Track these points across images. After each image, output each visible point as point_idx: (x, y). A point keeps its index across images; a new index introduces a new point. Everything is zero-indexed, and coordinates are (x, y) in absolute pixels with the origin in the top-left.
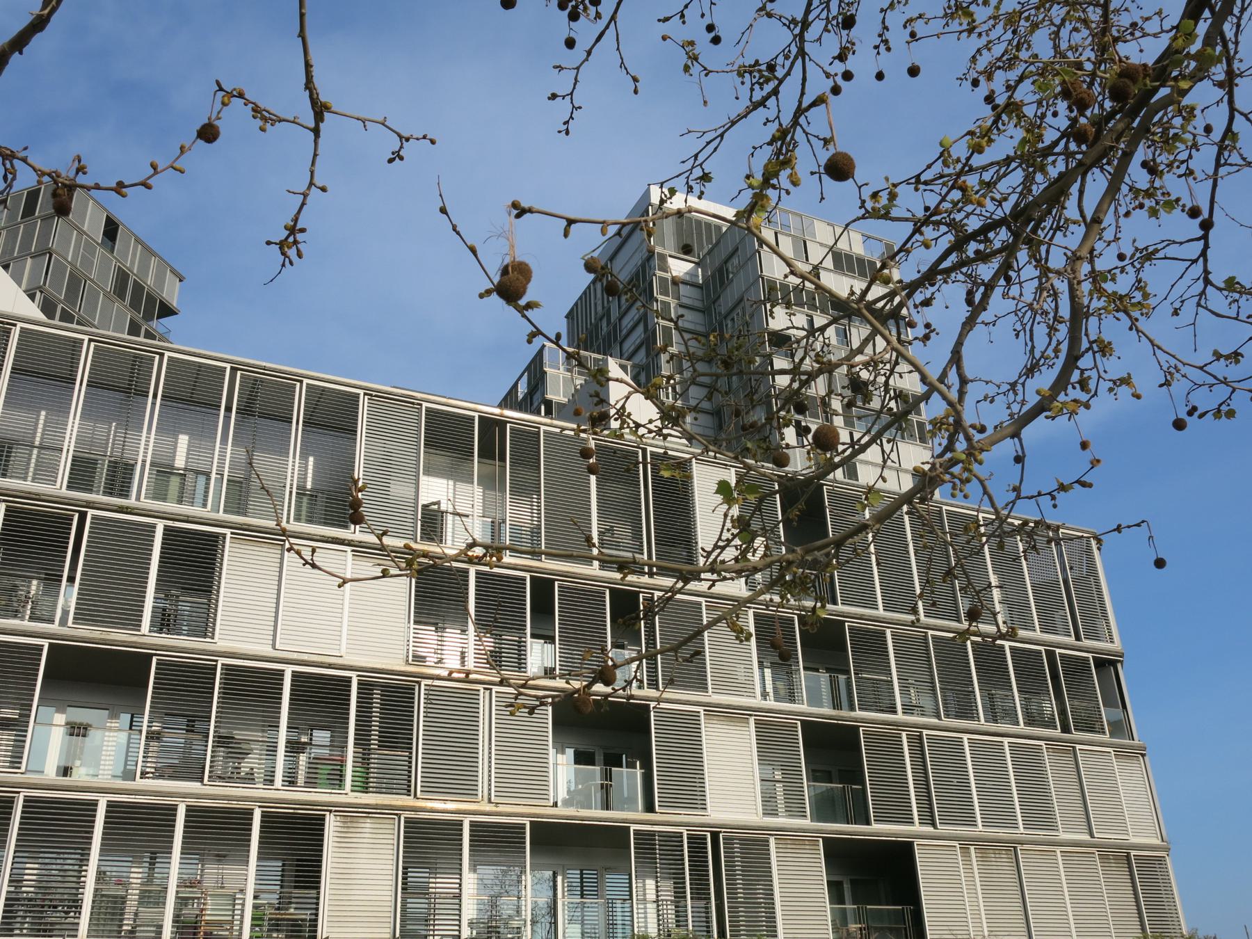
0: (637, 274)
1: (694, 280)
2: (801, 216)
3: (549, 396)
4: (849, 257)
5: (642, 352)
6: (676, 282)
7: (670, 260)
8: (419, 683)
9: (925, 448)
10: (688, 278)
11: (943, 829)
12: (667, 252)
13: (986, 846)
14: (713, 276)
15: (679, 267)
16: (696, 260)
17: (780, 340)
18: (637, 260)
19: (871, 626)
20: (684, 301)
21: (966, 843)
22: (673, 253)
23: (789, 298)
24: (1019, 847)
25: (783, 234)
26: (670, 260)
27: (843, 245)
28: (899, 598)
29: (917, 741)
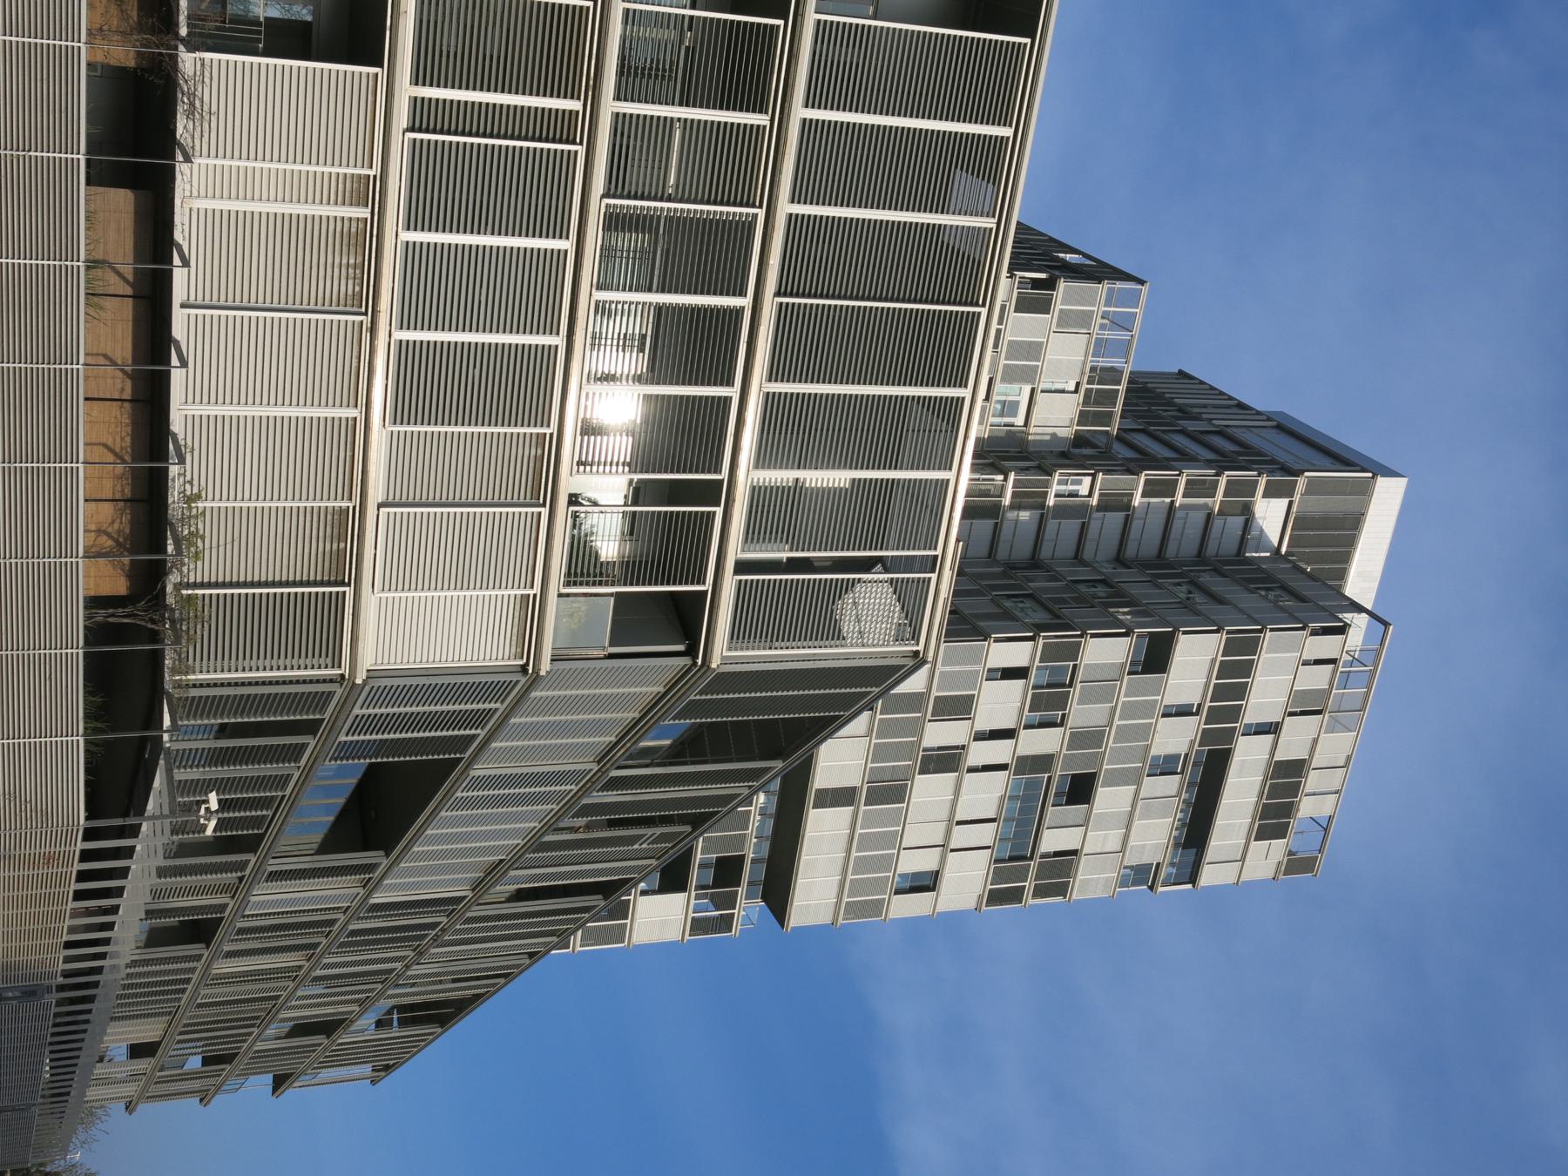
0: (1260, 454)
1: (1251, 543)
2: (1363, 709)
3: (1062, 285)
4: (1294, 790)
5: (1130, 454)
6: (1247, 511)
7: (1285, 502)
8: (544, 505)
9: (980, 897)
10: (1254, 533)
11: (401, 141)
12: (1297, 498)
13: (363, 243)
14: (1263, 571)
15: (1270, 515)
16: (1284, 550)
17: (1155, 658)
18: (1282, 457)
19: (776, 82)
20: (1218, 523)
21: (367, 192)
22: (1295, 509)
23: (1233, 678)
24: (367, 320)
25: (1334, 672)
26: (1285, 502)
27: (1312, 781)
28: (833, 163)
29: (562, 128)
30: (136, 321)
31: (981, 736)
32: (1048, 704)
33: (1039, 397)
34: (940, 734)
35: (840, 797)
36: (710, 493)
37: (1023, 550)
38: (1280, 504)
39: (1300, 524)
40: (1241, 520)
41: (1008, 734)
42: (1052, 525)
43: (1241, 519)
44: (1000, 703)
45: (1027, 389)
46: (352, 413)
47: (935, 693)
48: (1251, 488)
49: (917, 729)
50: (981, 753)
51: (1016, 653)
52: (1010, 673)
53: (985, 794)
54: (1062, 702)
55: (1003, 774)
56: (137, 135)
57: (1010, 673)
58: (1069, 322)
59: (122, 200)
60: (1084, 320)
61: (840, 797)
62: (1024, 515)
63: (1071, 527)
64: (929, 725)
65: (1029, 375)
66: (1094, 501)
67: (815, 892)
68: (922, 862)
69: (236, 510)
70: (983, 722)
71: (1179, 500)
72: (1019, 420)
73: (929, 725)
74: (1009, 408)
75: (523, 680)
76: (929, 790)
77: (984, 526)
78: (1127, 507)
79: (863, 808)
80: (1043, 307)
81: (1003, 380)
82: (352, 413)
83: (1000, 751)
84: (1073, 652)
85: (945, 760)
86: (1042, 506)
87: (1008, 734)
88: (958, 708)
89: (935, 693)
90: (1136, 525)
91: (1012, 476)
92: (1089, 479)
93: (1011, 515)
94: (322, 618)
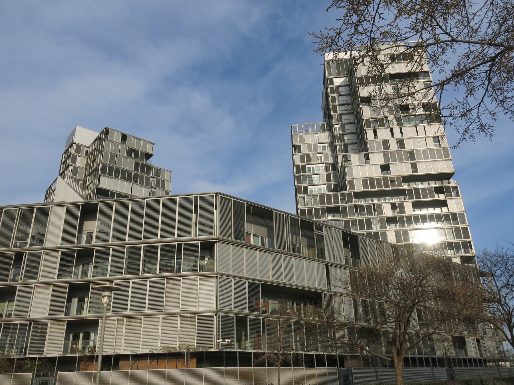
6: (338, 87)
12: (332, 77)
13: (130, 318)
19: (104, 248)
30: (143, 360)
31: (393, 137)
32: (381, 122)
33: (320, 141)
34: (394, 146)
35: (414, 167)
36: (180, 246)
37: (354, 136)
38: (335, 80)
39: (339, 76)
40: (340, 88)
41: (392, 130)
42: (347, 131)
43: (340, 88)
44: (384, 134)
45: (319, 145)
46: (161, 318)
47: (383, 150)
48: (332, 89)
49: (392, 153)
50: (397, 135)
51: (370, 134)
52: (375, 134)
53: (409, 131)
54: (381, 120)
55: (403, 128)
56: (111, 362)
57: (375, 134)
58: (302, 140)
59: (121, 363)
60: (301, 137)
61: (414, 167)
62: (346, 138)
63: (347, 127)
64: (391, 150)
65: (315, 146)
66: (340, 123)
67: (442, 167)
68: (430, 141)
69: (182, 337)
70: (389, 136)
71: (337, 103)
72: (326, 145)
73: (391, 150)
74: (324, 148)
75: (219, 276)
76: (409, 146)
77: (350, 147)
78: (340, 115)
79: (416, 161)
80: (299, 146)
81: (317, 150)
82: (161, 318)
83: (396, 131)
84: (368, 121)
85: (401, 143)
86: (343, 135)
87: (392, 130)
88: (386, 144)
89: (383, 150)
90: (344, 112)
91: (337, 144)
92: (335, 126)
93: (346, 141)
94: (204, 320)
